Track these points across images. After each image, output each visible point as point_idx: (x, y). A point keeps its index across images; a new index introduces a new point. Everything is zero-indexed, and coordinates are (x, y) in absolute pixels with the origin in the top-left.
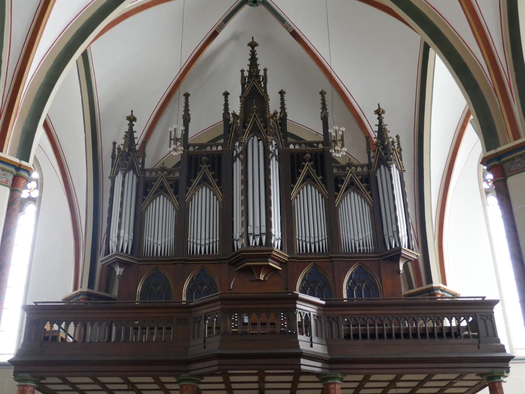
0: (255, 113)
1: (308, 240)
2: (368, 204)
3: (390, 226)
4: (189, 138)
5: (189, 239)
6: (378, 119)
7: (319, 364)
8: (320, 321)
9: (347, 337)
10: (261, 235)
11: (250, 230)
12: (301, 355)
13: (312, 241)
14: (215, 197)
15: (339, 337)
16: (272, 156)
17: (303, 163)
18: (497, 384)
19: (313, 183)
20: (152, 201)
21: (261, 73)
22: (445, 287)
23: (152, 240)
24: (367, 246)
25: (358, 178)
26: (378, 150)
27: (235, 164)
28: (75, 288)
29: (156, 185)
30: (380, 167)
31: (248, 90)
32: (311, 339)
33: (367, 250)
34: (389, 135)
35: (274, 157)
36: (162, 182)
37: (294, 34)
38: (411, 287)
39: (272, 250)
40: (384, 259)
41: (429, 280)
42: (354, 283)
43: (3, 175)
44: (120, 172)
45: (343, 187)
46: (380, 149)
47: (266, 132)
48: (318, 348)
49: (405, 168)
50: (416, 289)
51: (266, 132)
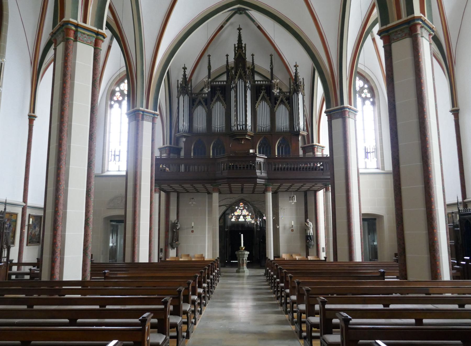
0: (240, 68)
1: (262, 126)
2: (288, 110)
3: (296, 121)
4: (211, 72)
5: (212, 126)
6: (295, 69)
7: (263, 180)
8: (265, 164)
9: (275, 169)
10: (243, 125)
11: (238, 123)
12: (257, 178)
13: (264, 126)
14: (223, 106)
15: (272, 170)
16: (248, 88)
17: (261, 91)
18: (328, 187)
19: (266, 100)
20: (196, 108)
21: (243, 45)
22: (319, 144)
23: (197, 126)
24: (286, 129)
25: (285, 98)
26: (294, 86)
27: (232, 91)
28: (164, 144)
29: (197, 101)
30: (294, 94)
31: (237, 55)
32: (261, 171)
33: (286, 130)
34: (300, 78)
35: (249, 89)
36: (200, 99)
37: (259, 27)
38: (305, 144)
39: (247, 132)
40: (293, 135)
41: (313, 142)
42: (280, 145)
43: (89, 38)
44: (181, 95)
45: (278, 102)
46: (295, 85)
47: (246, 77)
48: (264, 175)
49: (305, 94)
50: (307, 145)
51: (246, 77)
